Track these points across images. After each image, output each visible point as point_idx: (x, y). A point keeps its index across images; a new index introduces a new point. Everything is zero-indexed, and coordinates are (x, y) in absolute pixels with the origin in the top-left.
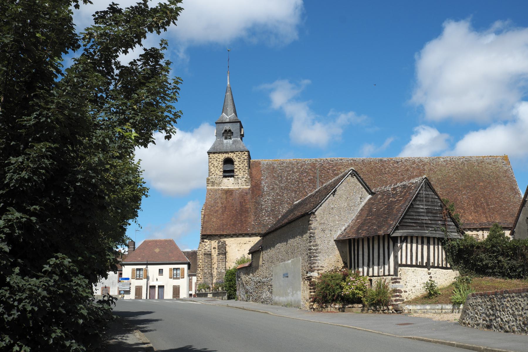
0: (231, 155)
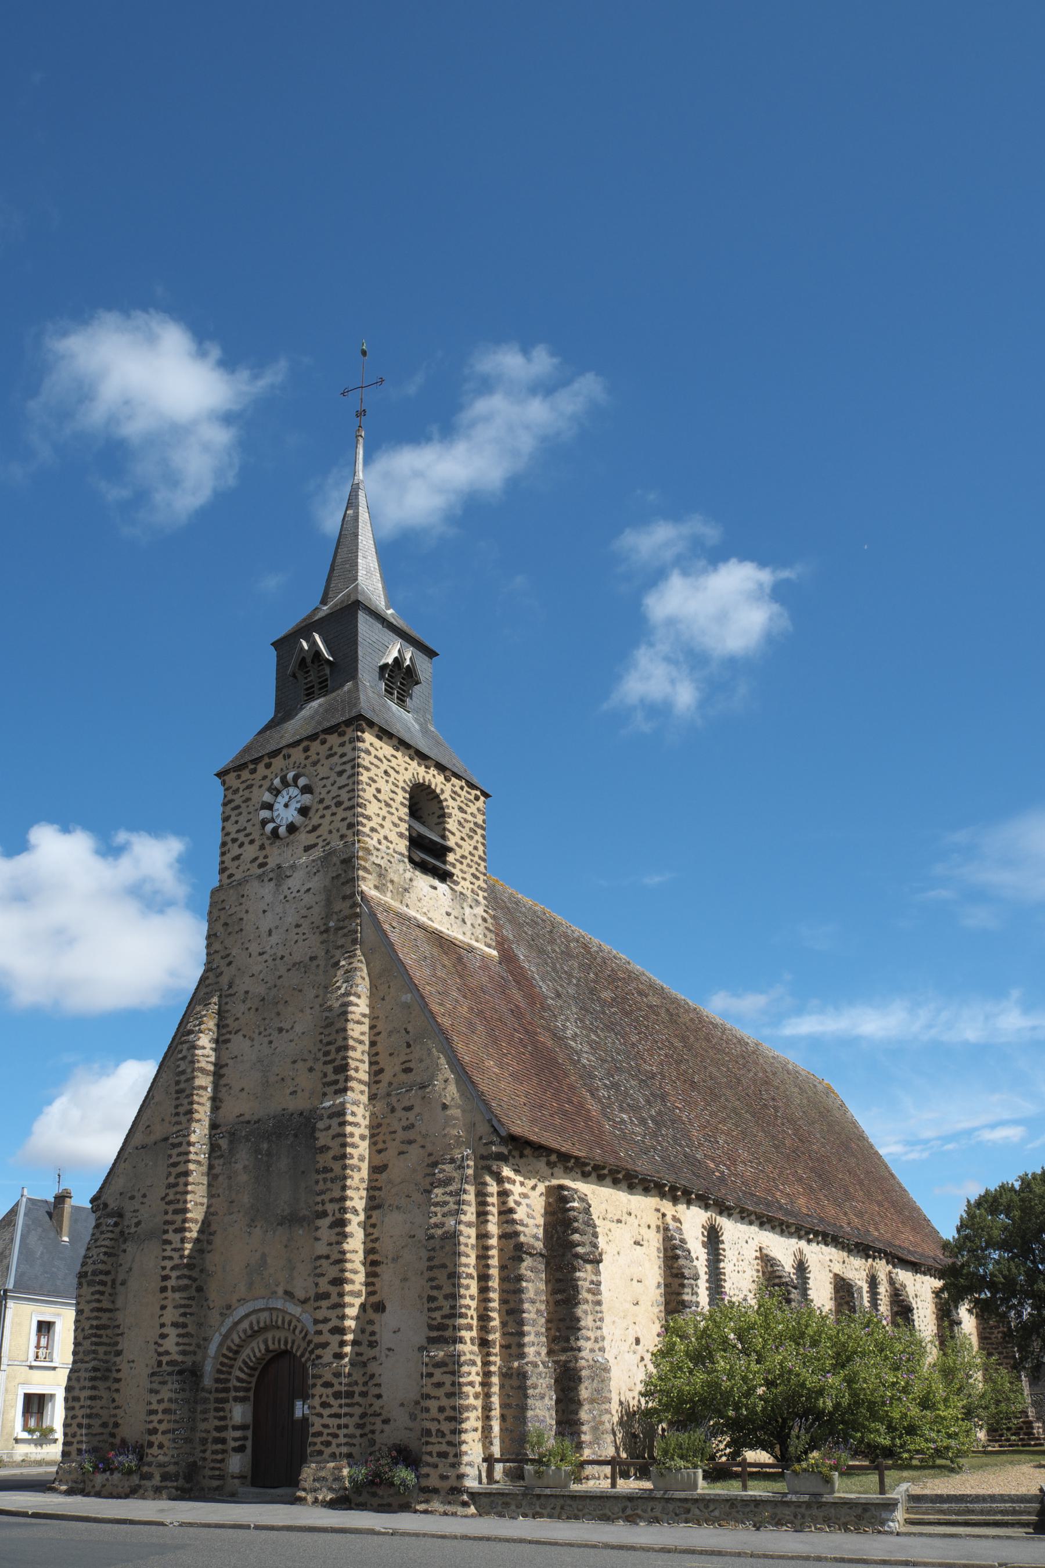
0: (436, 780)
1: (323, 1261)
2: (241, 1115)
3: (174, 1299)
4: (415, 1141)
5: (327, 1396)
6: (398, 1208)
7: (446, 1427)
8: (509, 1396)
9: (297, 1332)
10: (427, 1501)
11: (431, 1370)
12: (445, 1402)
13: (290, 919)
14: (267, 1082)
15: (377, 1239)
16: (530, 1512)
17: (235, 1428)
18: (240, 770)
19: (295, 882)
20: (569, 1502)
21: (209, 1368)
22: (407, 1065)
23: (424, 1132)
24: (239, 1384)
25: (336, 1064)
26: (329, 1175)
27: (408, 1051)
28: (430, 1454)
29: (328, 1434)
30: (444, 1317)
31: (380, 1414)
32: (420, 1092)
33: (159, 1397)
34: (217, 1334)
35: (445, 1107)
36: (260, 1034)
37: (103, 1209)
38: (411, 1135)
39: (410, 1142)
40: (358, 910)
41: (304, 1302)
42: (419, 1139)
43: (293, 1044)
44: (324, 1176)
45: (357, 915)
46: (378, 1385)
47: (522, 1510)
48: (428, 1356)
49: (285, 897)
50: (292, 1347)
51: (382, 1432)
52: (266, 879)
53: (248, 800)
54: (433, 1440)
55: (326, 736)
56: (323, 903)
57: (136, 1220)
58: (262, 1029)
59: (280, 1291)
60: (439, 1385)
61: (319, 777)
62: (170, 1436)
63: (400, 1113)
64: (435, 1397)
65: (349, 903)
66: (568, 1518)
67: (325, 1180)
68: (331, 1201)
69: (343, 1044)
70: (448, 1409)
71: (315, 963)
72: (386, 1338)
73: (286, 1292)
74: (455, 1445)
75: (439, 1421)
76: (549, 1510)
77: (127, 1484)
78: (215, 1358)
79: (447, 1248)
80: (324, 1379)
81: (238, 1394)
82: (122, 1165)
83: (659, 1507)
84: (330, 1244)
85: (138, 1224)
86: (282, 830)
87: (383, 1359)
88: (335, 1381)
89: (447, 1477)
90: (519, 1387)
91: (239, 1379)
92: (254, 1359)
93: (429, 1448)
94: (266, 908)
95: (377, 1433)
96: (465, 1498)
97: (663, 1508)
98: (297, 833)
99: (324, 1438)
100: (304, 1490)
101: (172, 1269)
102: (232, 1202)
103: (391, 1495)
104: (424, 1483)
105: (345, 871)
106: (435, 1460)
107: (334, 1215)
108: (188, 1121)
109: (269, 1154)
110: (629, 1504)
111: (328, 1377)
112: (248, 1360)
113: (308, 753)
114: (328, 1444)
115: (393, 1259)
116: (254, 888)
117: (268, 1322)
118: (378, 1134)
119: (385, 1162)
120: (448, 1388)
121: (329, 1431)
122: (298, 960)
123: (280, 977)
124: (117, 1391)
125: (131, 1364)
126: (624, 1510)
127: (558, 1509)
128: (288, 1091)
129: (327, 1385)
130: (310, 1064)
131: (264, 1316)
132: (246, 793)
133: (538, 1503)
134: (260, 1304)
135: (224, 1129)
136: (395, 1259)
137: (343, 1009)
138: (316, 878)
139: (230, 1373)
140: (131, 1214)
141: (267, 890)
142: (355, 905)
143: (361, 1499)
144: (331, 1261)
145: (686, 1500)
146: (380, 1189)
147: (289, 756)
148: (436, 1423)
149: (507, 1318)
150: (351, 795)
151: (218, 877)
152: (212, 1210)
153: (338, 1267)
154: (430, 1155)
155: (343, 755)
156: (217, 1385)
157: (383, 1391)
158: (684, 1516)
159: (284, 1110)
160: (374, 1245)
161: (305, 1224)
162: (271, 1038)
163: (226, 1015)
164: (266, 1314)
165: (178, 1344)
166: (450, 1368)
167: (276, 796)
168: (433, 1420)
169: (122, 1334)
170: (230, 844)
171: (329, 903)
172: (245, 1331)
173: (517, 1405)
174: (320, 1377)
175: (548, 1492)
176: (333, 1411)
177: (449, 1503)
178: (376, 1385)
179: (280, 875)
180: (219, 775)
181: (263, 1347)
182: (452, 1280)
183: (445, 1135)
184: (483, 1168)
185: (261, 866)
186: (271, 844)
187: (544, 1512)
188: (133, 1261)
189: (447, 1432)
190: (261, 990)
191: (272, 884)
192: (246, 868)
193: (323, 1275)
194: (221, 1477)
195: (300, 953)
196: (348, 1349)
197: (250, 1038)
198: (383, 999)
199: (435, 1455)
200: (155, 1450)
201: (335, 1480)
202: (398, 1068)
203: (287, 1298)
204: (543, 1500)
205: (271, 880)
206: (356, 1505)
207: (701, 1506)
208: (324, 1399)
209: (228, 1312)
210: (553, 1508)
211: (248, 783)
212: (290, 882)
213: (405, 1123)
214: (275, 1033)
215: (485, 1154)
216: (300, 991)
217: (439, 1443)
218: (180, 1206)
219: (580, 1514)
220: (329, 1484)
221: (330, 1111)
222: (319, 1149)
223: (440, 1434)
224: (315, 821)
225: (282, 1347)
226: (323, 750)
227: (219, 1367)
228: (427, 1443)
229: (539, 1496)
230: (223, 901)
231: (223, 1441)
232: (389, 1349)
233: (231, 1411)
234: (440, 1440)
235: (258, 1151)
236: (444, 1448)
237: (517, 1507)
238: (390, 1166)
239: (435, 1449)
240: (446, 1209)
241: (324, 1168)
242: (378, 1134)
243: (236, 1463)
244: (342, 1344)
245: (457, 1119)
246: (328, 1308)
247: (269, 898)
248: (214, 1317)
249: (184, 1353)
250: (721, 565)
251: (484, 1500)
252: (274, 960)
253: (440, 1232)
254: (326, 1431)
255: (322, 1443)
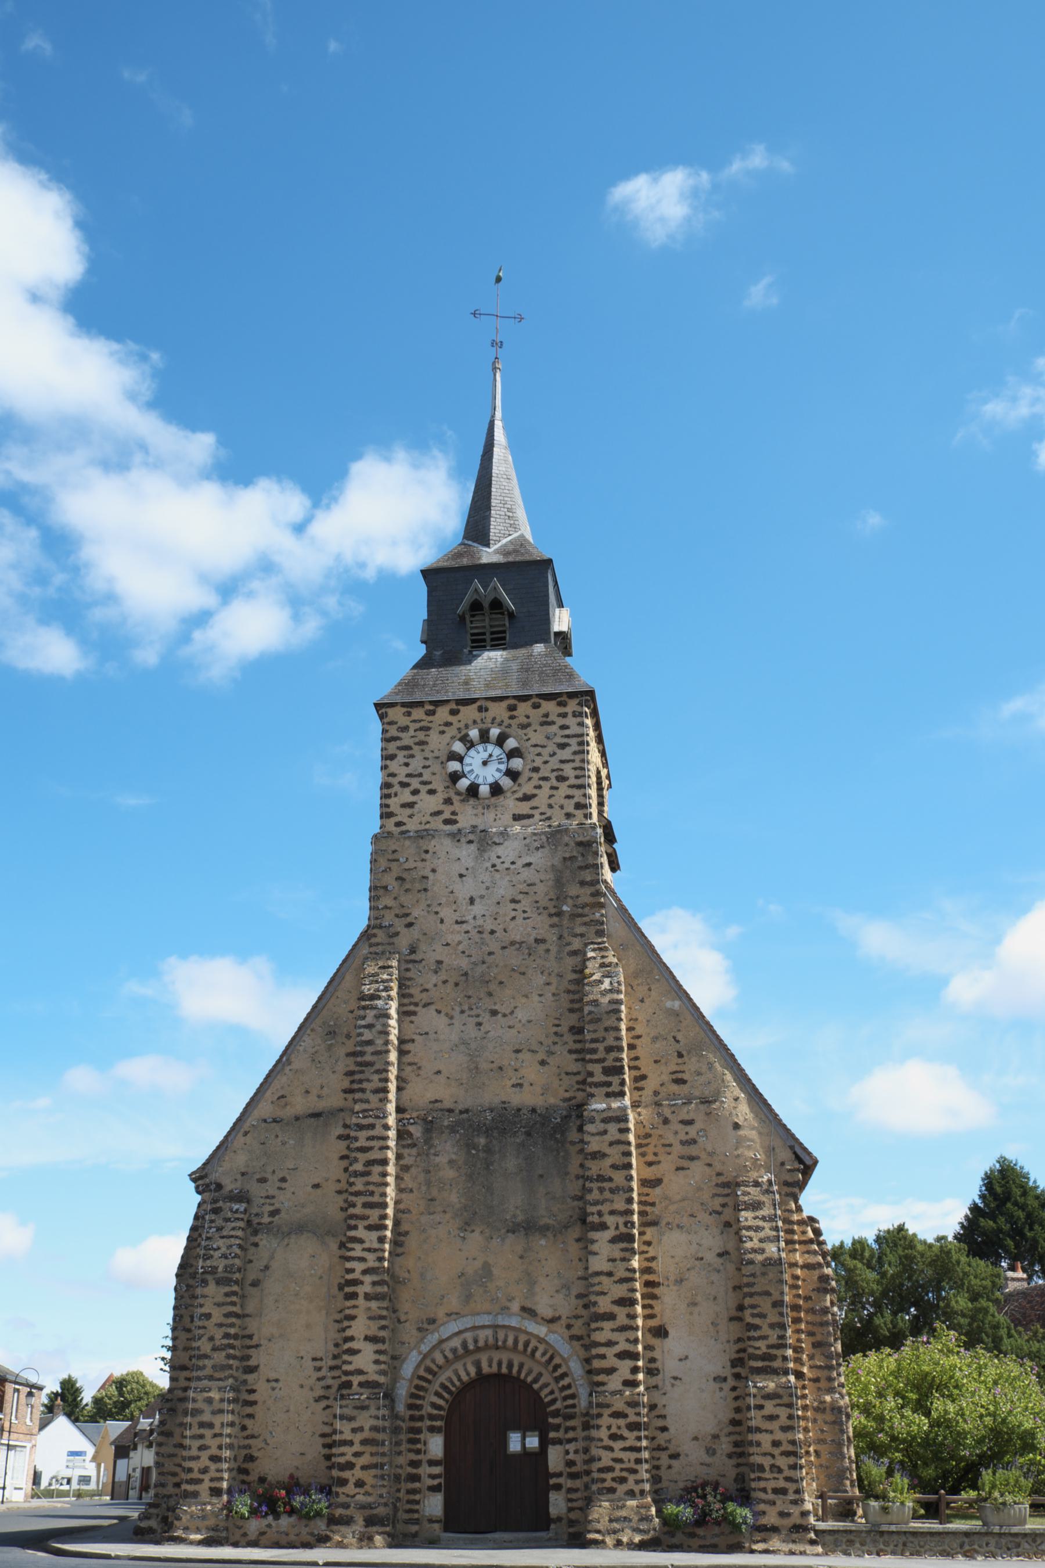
1: (604, 1279)
2: (436, 1101)
3: (369, 1309)
4: (697, 1158)
5: (619, 1428)
6: (678, 1226)
7: (782, 1462)
8: (822, 1431)
9: (538, 1354)
10: (764, 1541)
11: (762, 1402)
12: (779, 1436)
13: (502, 892)
14: (477, 1068)
15: (653, 1258)
16: (874, 1550)
17: (432, 1463)
18: (411, 707)
19: (508, 851)
20: (911, 1539)
21: (402, 1391)
22: (680, 1076)
23: (709, 1149)
24: (435, 1412)
25: (606, 1064)
26: (606, 1185)
27: (680, 1061)
28: (764, 1490)
29: (622, 1470)
30: (769, 1347)
31: (666, 1449)
32: (702, 1107)
33: (355, 1425)
34: (414, 1353)
35: (737, 1126)
36: (462, 1012)
37: (216, 1191)
38: (693, 1150)
39: (692, 1158)
40: (602, 900)
41: (552, 1321)
42: (703, 1155)
43: (514, 1031)
44: (599, 1184)
45: (602, 906)
46: (664, 1417)
47: (865, 1548)
48: (755, 1386)
49: (494, 866)
50: (519, 1372)
51: (670, 1467)
52: (463, 840)
53: (422, 743)
54: (767, 1475)
55: (541, 701)
56: (550, 883)
57: (272, 1208)
58: (466, 1007)
59: (515, 1307)
60: (771, 1418)
61: (530, 742)
62: (373, 1472)
63: (675, 1126)
64: (766, 1431)
65: (589, 890)
66: (912, 1554)
67: (601, 1190)
68: (612, 1213)
69: (615, 1044)
70: (785, 1443)
71: (542, 947)
72: (670, 1366)
73: (524, 1309)
74: (797, 1481)
75: (773, 1456)
76: (892, 1547)
77: (304, 1531)
78: (411, 1381)
79: (771, 1276)
80: (614, 1409)
81: (434, 1423)
82: (240, 1140)
83: (993, 1541)
84: (613, 1260)
85: (274, 1213)
86: (464, 783)
87: (668, 1388)
88: (629, 1411)
89: (788, 1515)
90: (834, 1423)
91: (434, 1406)
92: (458, 1383)
93: (762, 1484)
94: (464, 872)
95: (663, 1468)
96: (812, 1535)
97: (997, 1543)
98: (501, 798)
99: (617, 1474)
100: (598, 1532)
101: (365, 1272)
102: (432, 1200)
103: (716, 1535)
104: (764, 1521)
105: (583, 855)
106: (771, 1496)
107: (617, 1228)
108: (381, 1100)
109: (488, 1150)
110: (966, 1540)
111: (619, 1405)
112: (449, 1384)
113: (514, 713)
114: (623, 1480)
115: (676, 1281)
116: (442, 846)
117: (491, 1341)
118: (647, 1145)
119: (659, 1176)
120: (783, 1420)
121: (624, 1466)
122: (518, 938)
123: (490, 954)
124: (251, 1416)
125: (274, 1384)
126: (962, 1546)
127: (900, 1547)
128: (510, 1083)
129: (617, 1415)
130: (541, 1056)
131: (483, 1335)
132: (421, 736)
133: (881, 1540)
134: (485, 1320)
135: (415, 1115)
136: (680, 1281)
137: (615, 1006)
138: (539, 854)
139: (423, 1398)
140: (263, 1201)
141: (466, 853)
142: (598, 893)
143: (674, 1541)
144: (616, 1278)
145: (1016, 1535)
146: (653, 1204)
147: (487, 710)
148: (769, 1458)
149: (813, 1351)
150: (579, 773)
151: (379, 823)
152: (402, 1206)
153: (625, 1286)
154: (719, 1174)
155: (564, 727)
156: (411, 1412)
157: (669, 1423)
158: (1015, 1550)
159: (504, 1103)
160: (650, 1264)
161: (549, 1234)
162: (480, 1019)
163: (409, 983)
164: (489, 1332)
165: (377, 1362)
166: (786, 1400)
167: (468, 749)
168: (765, 1454)
169: (257, 1346)
170: (397, 788)
171: (559, 883)
172: (454, 1350)
173: (833, 1441)
174: (608, 1406)
175: (893, 1528)
176: (627, 1444)
177: (794, 1542)
178: (658, 1417)
179: (483, 840)
180: (378, 706)
181: (473, 1371)
182: (779, 1309)
183: (738, 1156)
184: (787, 1195)
185: (447, 822)
186: (463, 801)
187: (889, 1549)
188: (272, 1257)
189: (785, 1467)
190: (464, 963)
191: (473, 847)
192: (424, 820)
193: (604, 1294)
194: (417, 1522)
195: (519, 931)
196: (641, 1376)
197: (447, 1015)
198: (642, 1001)
199: (770, 1491)
200: (350, 1489)
201: (641, 1520)
202: (666, 1078)
203: (525, 1315)
204: (886, 1537)
205: (470, 842)
206: (668, 1546)
207: (1030, 1540)
208: (614, 1430)
209: (431, 1327)
210: (896, 1546)
211: (422, 724)
212: (499, 850)
213: (682, 1136)
214: (487, 1016)
215: (790, 1180)
216: (524, 974)
217: (775, 1478)
218: (376, 1199)
219: (923, 1550)
220: (634, 1524)
221: (605, 1115)
222: (590, 1154)
223: (775, 1469)
224: (528, 789)
225: (504, 1370)
226: (536, 715)
227: (413, 1390)
228: (760, 1479)
229: (882, 1533)
230: (394, 852)
231: (415, 1478)
232: (675, 1378)
233: (425, 1444)
234: (776, 1475)
235: (470, 1146)
236: (782, 1484)
237: (862, 1545)
238: (665, 1180)
239: (771, 1485)
240: (762, 1235)
241: (599, 1176)
242: (647, 1145)
243: (434, 1505)
244: (635, 1370)
245: (752, 1140)
246: (613, 1330)
247: (470, 863)
248: (409, 1332)
249: (382, 1373)
250: (71, 320)
251: (828, 1538)
252: (480, 932)
253: (760, 1258)
254: (618, 1466)
255: (613, 1479)
